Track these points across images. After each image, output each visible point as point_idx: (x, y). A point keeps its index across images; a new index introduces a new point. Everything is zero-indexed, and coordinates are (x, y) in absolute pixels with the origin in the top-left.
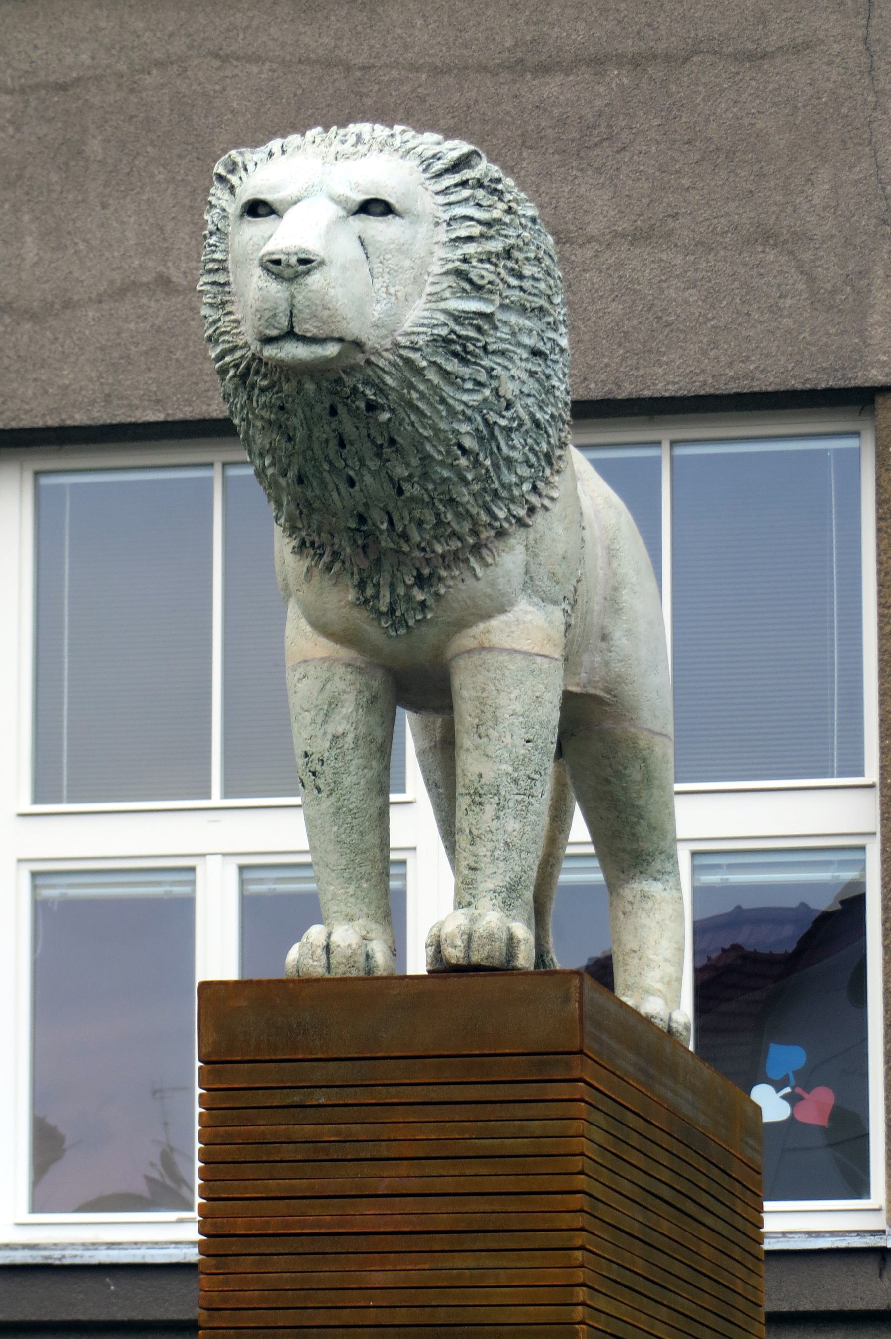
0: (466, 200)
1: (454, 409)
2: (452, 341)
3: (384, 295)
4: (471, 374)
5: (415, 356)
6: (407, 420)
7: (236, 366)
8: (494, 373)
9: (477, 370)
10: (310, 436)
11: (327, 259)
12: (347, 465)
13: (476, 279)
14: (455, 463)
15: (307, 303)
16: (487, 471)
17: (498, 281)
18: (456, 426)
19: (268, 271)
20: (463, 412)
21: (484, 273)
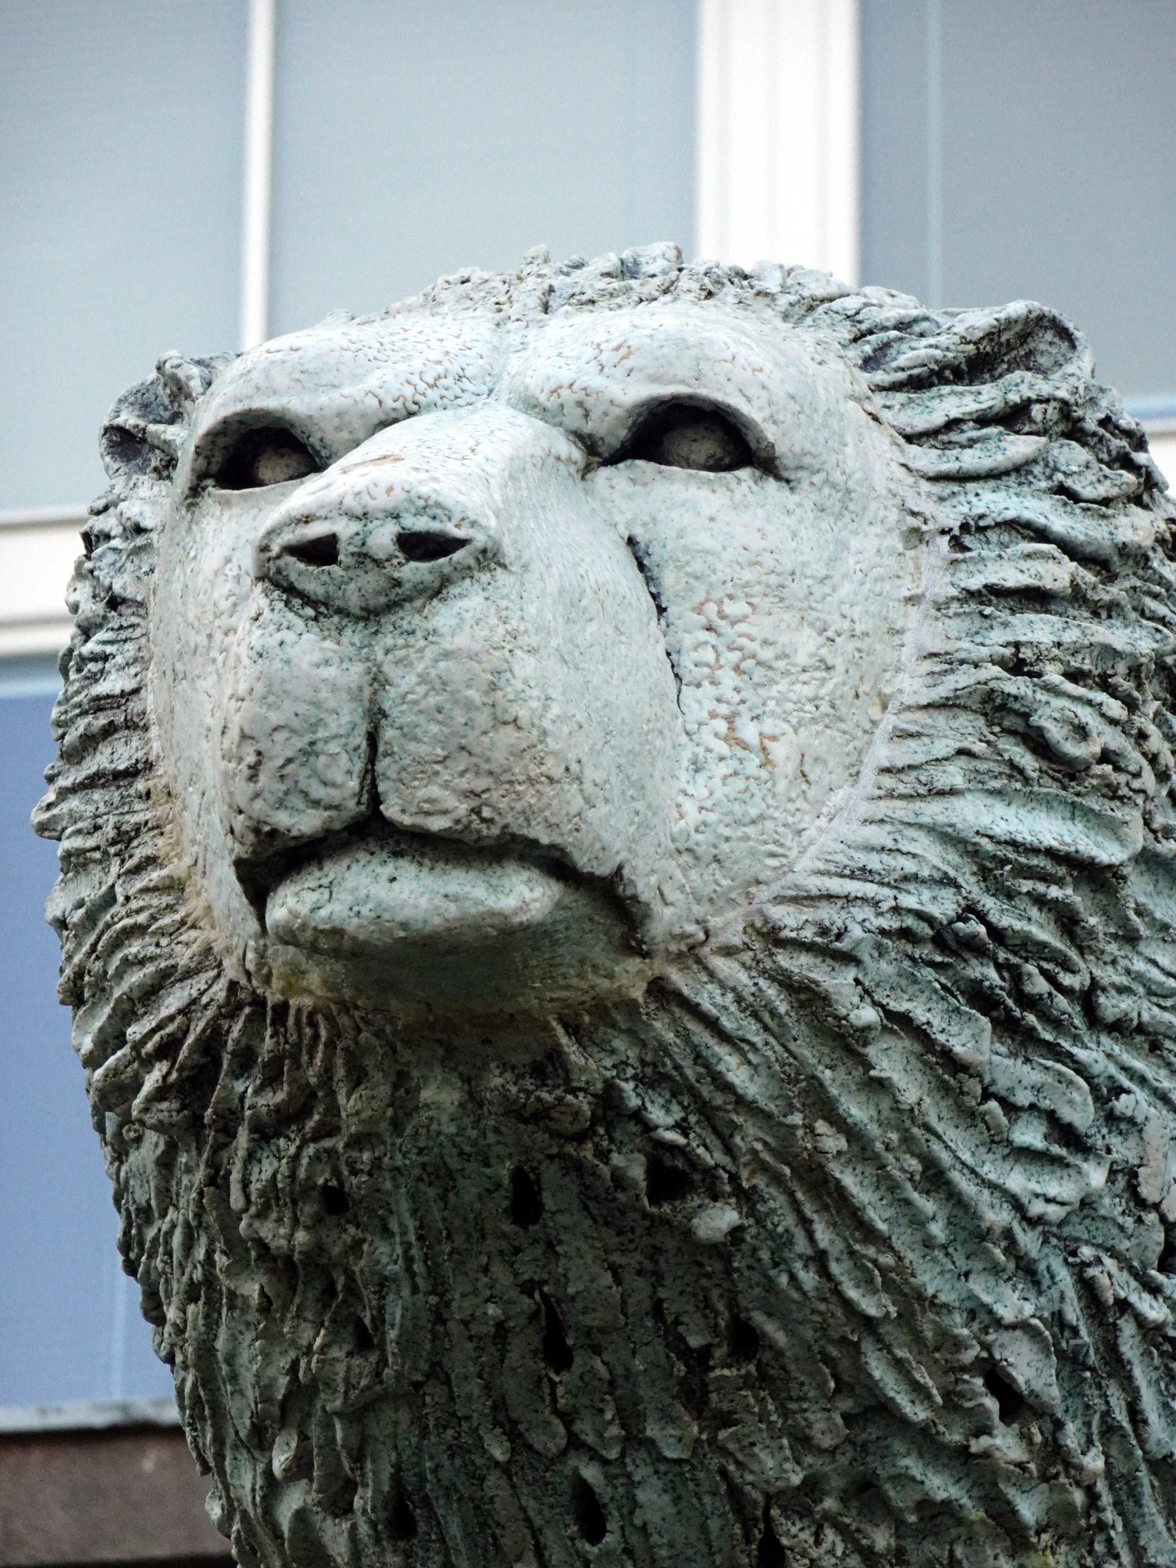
0: (1020, 470)
1: (976, 1216)
2: (971, 947)
3: (722, 748)
4: (1038, 1089)
5: (839, 983)
6: (801, 1245)
7: (167, 1050)
8: (1123, 1105)
9: (1060, 1078)
10: (439, 1318)
11: (509, 552)
12: (575, 1443)
13: (1056, 733)
14: (976, 1446)
15: (433, 700)
16: (1092, 1496)
17: (1134, 758)
18: (981, 1288)
19: (290, 591)
20: (1008, 1234)
21: (1086, 715)
